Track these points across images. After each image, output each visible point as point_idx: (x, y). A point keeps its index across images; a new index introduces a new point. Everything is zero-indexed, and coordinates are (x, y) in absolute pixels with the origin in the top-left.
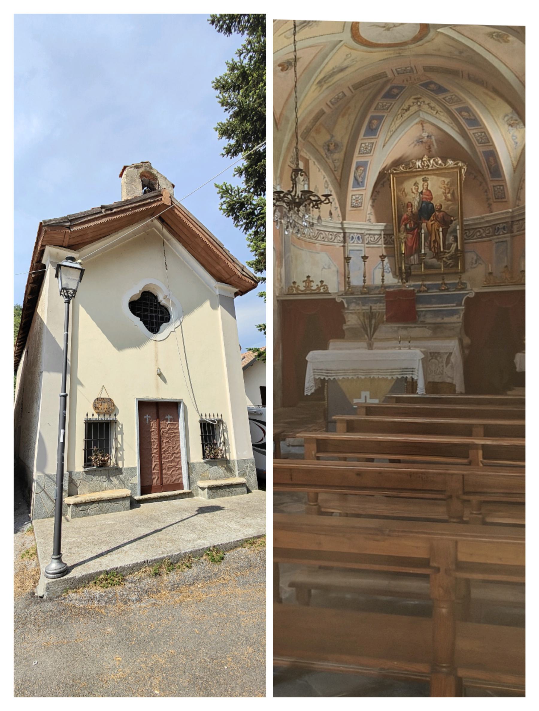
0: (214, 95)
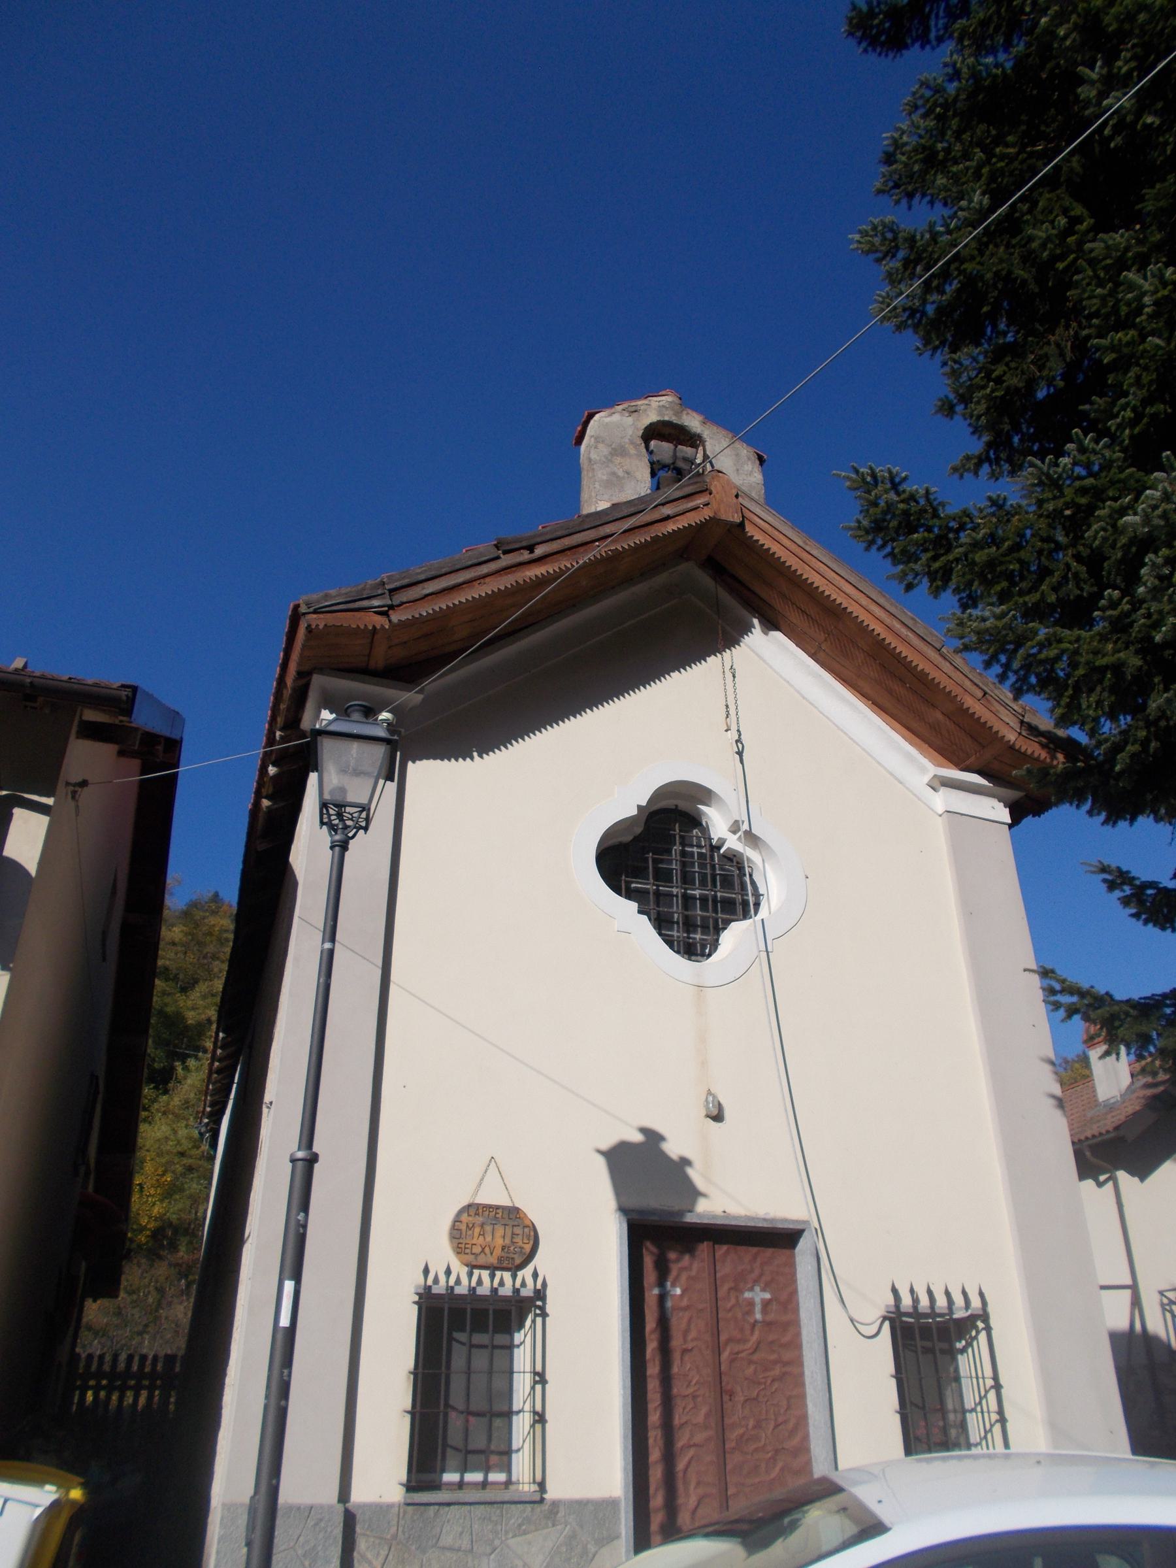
0: (852, 42)
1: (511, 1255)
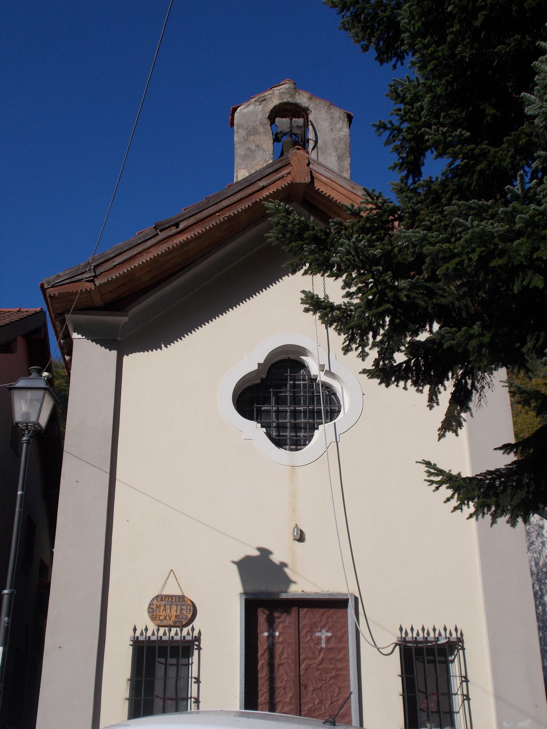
1: (180, 620)
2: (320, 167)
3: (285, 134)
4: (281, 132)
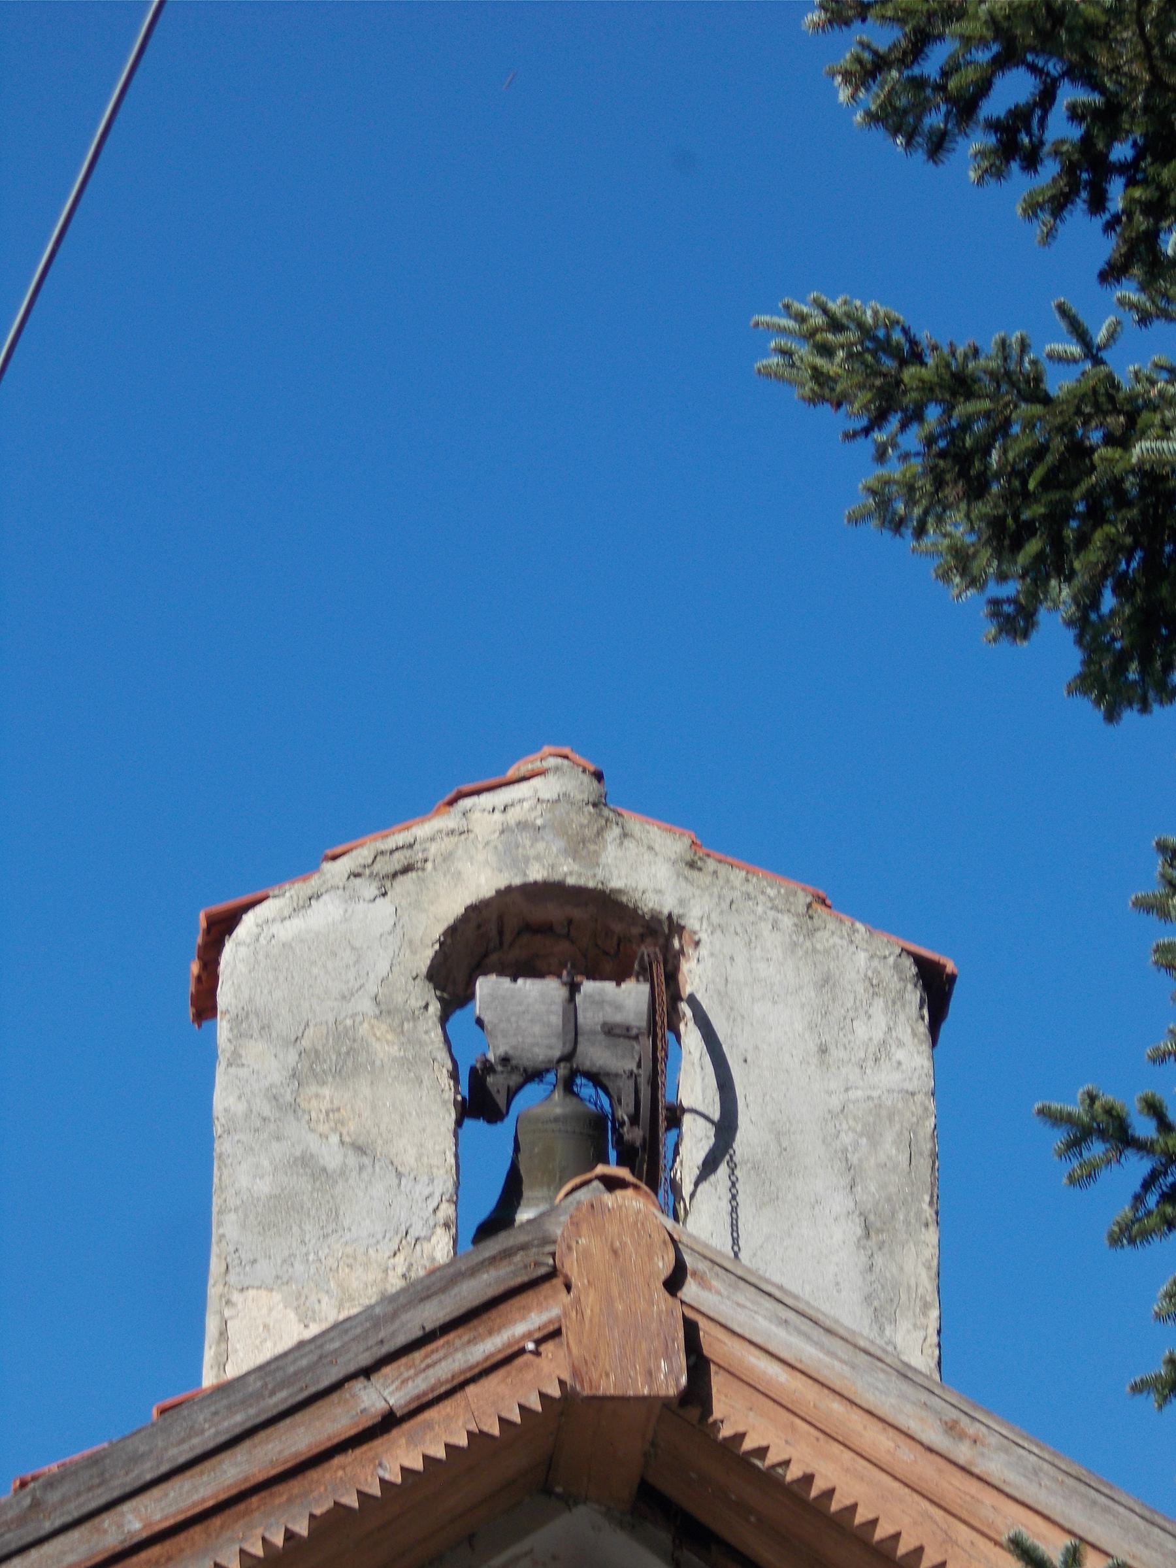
2: (746, 1296)
3: (534, 1075)
4: (505, 1060)
